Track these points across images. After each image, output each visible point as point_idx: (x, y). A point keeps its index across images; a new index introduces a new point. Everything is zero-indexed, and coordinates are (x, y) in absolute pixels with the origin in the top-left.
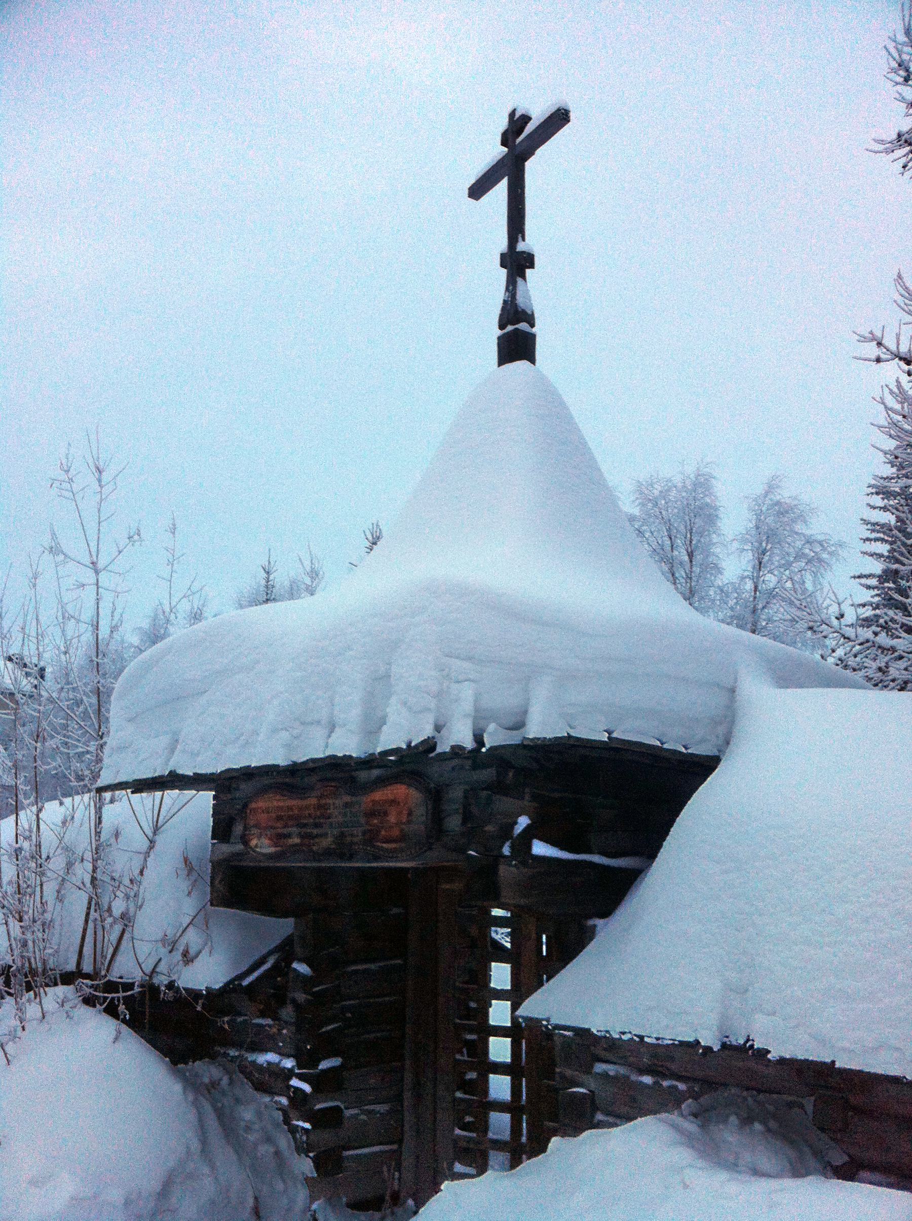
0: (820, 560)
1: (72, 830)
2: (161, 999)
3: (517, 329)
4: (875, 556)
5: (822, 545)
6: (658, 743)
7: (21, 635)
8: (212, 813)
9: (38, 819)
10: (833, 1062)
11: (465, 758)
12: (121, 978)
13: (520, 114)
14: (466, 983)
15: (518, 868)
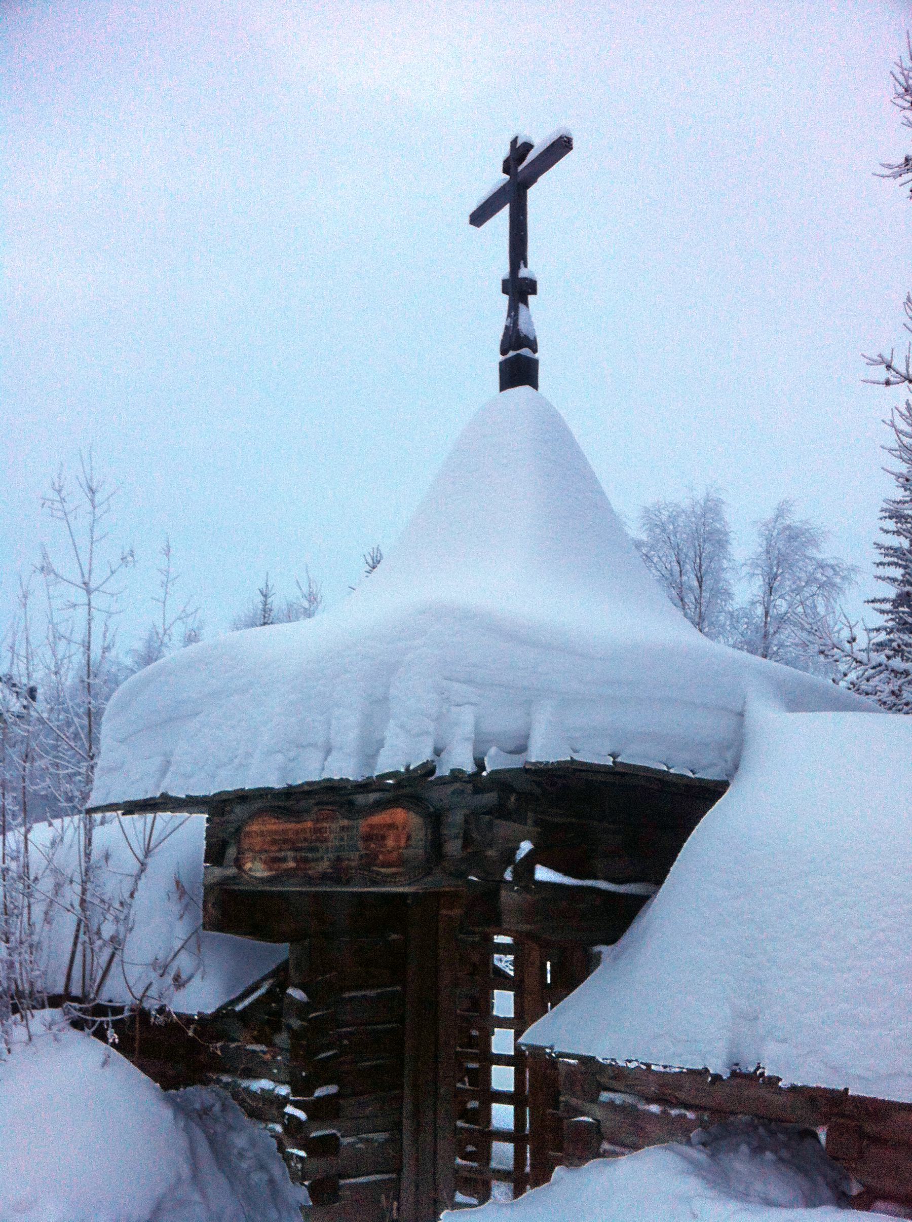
0: (834, 585)
1: (61, 850)
2: (152, 1024)
3: (518, 355)
4: (888, 580)
5: (834, 570)
6: (665, 768)
7: (10, 654)
8: (205, 836)
9: (26, 839)
10: (846, 1090)
11: (464, 782)
12: (111, 1001)
13: (521, 143)
14: (468, 1010)
15: (520, 894)
